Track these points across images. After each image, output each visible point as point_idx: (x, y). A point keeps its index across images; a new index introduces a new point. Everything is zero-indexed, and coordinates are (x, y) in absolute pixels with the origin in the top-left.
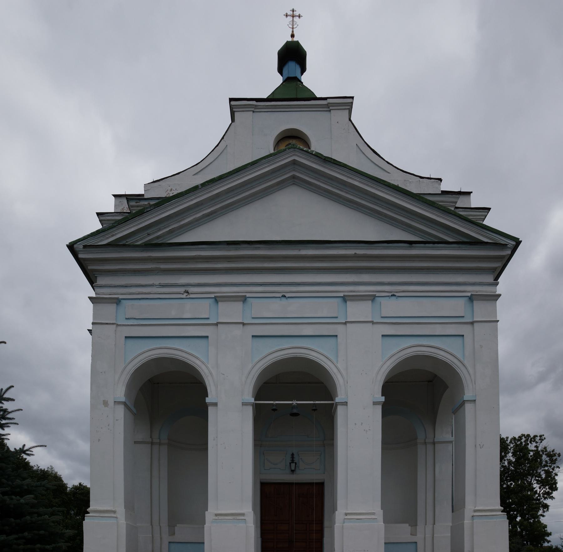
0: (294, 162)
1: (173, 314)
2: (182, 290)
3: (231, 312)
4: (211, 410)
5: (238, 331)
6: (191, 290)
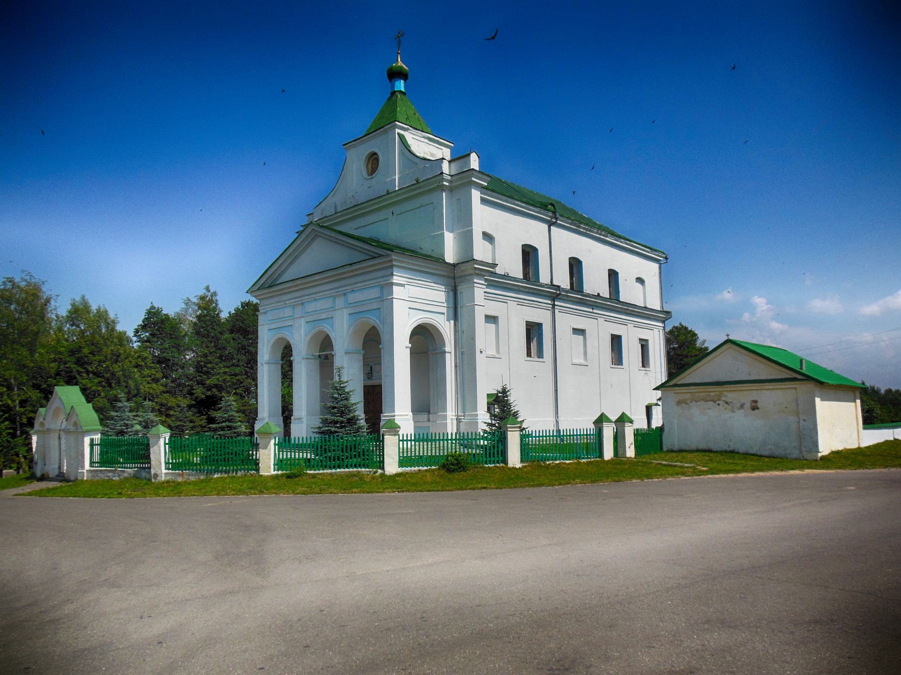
1: (282, 315)
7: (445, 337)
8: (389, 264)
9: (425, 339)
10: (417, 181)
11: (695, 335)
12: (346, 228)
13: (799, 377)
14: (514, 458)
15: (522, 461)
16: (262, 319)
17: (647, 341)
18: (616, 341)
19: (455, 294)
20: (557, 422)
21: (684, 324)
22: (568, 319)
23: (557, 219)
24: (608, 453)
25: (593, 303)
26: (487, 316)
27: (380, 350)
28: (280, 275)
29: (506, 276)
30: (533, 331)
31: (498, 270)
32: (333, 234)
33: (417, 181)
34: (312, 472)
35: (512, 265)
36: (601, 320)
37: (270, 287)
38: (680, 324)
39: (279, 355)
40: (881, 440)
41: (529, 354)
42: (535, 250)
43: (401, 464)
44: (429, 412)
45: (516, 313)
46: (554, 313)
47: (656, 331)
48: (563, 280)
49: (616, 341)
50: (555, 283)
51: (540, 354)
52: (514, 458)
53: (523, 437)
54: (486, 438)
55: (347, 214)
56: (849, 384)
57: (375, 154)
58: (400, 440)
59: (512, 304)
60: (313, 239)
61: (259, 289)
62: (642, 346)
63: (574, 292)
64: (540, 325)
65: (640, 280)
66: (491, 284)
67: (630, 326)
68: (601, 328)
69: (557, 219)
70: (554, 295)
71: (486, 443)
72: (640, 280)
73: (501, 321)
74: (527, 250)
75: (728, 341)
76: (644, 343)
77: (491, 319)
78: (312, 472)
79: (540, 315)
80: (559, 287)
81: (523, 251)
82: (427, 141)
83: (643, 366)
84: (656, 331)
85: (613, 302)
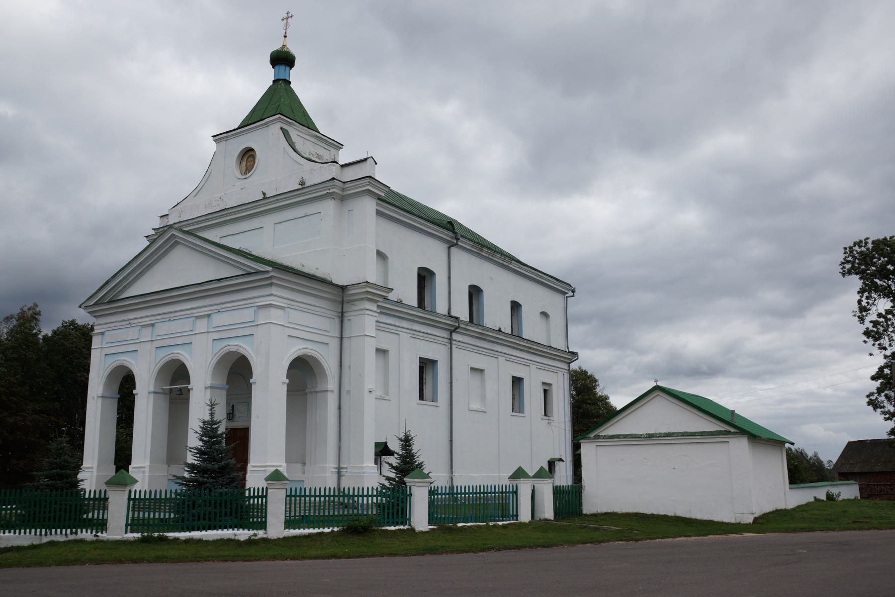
0: (368, 190)
1: (124, 338)
2: (127, 323)
3: (202, 325)
4: (253, 387)
5: (148, 345)
6: (132, 322)
7: (328, 373)
8: (269, 282)
9: (303, 372)
10: (302, 183)
11: (596, 381)
12: (213, 235)
13: (732, 430)
14: (420, 519)
15: (430, 523)
16: (96, 342)
17: (550, 385)
18: (517, 382)
19: (342, 322)
20: (452, 479)
21: (584, 368)
22: (466, 358)
23: (458, 239)
24: (525, 516)
25: (494, 337)
26: (378, 350)
27: (249, 386)
28: (126, 288)
29: (399, 303)
30: (426, 366)
31: (392, 296)
32: (198, 242)
33: (302, 183)
34: (392, 528)
35: (406, 291)
36: (502, 360)
37: (110, 302)
38: (580, 368)
39: (116, 386)
40: (803, 502)
41: (422, 397)
42: (432, 274)
43: (289, 524)
44: (304, 464)
45: (410, 347)
46: (451, 348)
47: (560, 374)
48: (461, 311)
49: (517, 382)
50: (453, 314)
51: (434, 399)
52: (420, 519)
53: (432, 492)
54: (384, 495)
55: (212, 219)
56: (771, 437)
57: (252, 150)
58: (287, 496)
59: (405, 336)
60: (172, 247)
61: (96, 304)
62: (545, 391)
63: (469, 325)
64: (433, 362)
65: (545, 314)
66: (384, 311)
67: (533, 367)
68: (501, 368)
69: (458, 239)
70: (453, 326)
71: (85, 516)
72: (545, 314)
73: (392, 355)
74: (423, 274)
75: (657, 388)
76: (546, 388)
77: (382, 352)
78: (392, 528)
79: (435, 351)
80: (457, 318)
81: (419, 275)
82: (313, 140)
83: (546, 415)
84: (560, 374)
85: (514, 339)
